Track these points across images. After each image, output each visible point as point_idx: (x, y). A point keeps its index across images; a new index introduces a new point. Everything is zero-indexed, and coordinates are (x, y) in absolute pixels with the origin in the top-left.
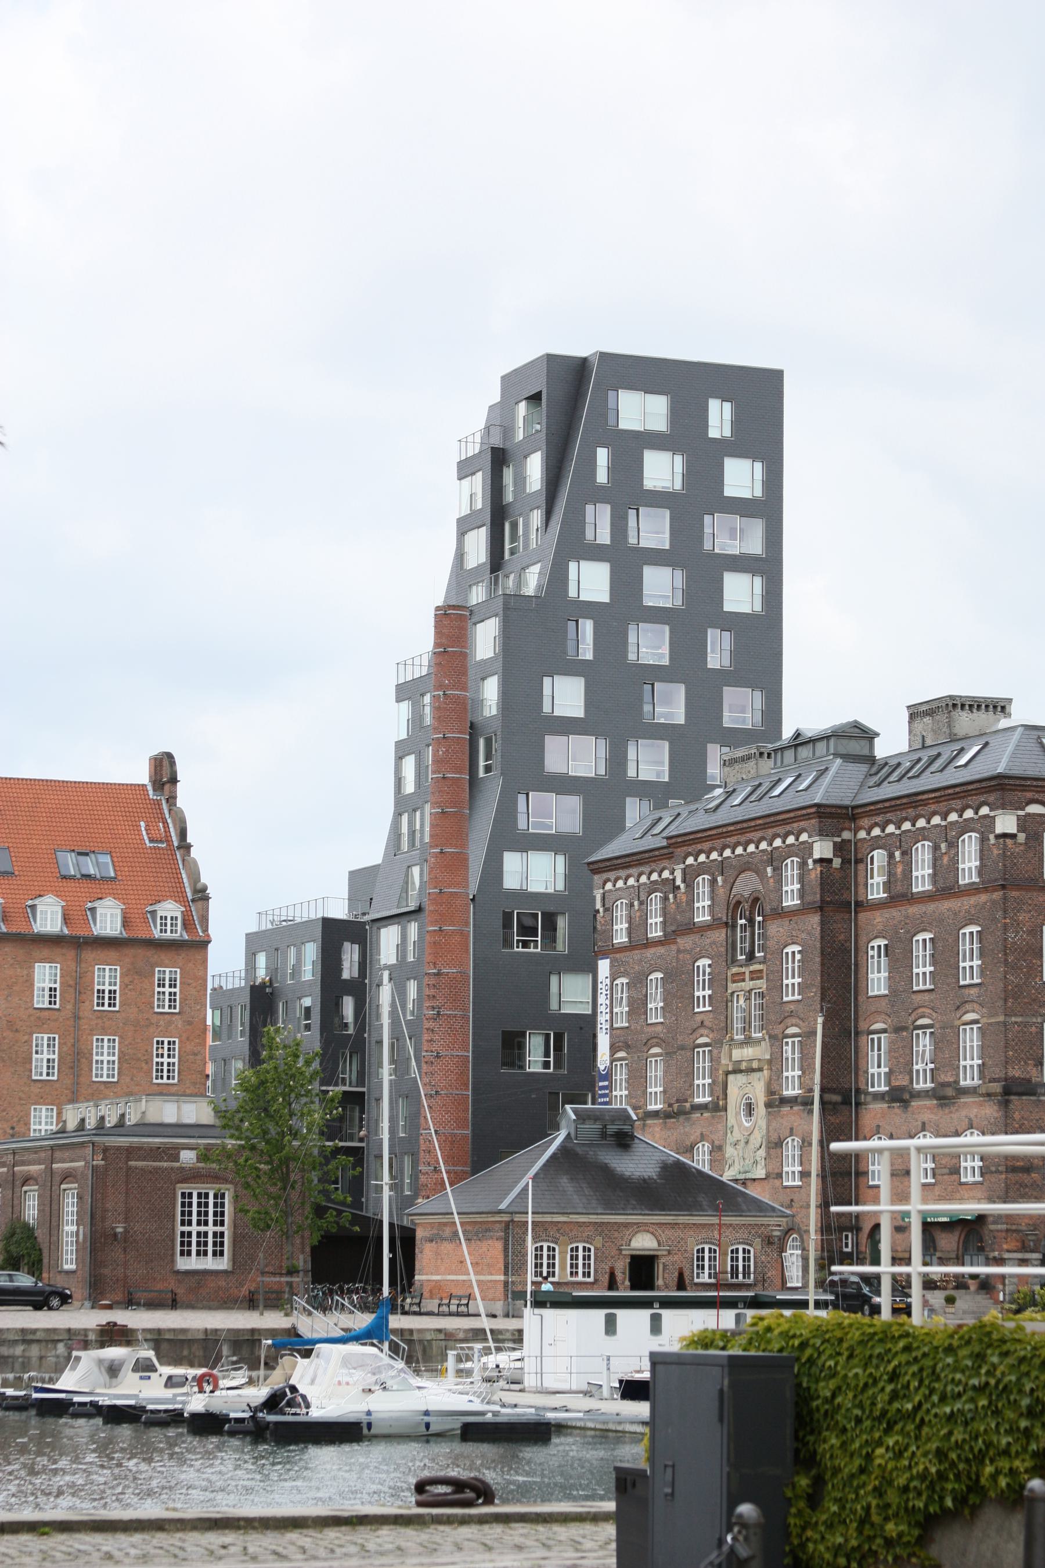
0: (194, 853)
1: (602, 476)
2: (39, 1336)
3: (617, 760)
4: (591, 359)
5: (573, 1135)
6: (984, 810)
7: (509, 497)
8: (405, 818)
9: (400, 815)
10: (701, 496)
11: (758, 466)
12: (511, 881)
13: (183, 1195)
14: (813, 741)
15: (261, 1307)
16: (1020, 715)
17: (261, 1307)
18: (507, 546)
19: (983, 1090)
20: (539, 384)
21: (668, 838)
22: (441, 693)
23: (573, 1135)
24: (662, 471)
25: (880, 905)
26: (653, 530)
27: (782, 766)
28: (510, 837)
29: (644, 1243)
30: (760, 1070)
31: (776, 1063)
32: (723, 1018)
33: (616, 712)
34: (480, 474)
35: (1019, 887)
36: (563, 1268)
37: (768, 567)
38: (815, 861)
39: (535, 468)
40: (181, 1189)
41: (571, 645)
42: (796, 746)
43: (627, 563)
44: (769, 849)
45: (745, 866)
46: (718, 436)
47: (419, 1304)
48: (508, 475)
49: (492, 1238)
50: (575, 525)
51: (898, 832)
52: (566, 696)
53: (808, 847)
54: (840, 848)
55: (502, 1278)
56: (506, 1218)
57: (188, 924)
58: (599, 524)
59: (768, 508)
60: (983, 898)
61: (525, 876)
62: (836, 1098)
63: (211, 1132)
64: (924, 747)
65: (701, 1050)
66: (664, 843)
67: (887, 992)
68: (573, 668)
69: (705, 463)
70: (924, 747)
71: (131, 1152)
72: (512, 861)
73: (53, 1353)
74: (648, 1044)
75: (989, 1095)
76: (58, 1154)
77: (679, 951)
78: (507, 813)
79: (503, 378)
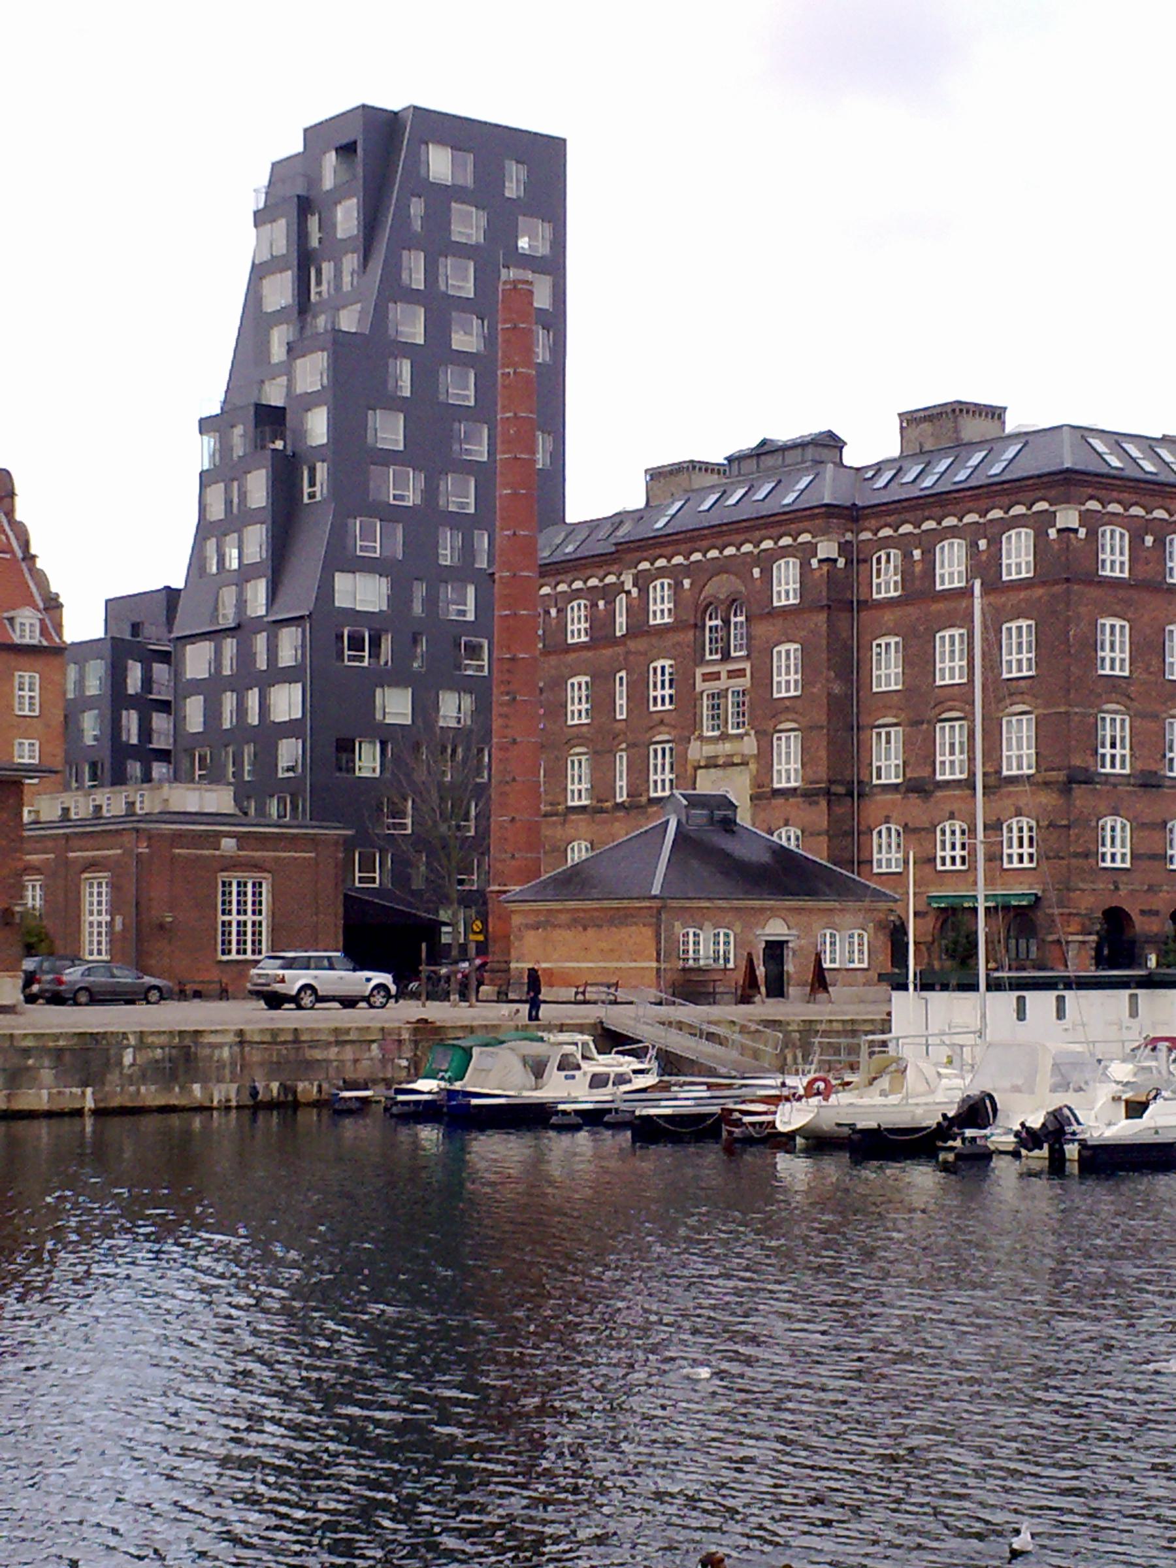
0: (39, 564)
1: (417, 225)
2: (353, 1036)
3: (431, 492)
5: (684, 820)
6: (805, 537)
7: (314, 243)
8: (211, 545)
9: (205, 539)
10: (495, 252)
13: (224, 883)
14: (785, 448)
15: (423, 998)
16: (1012, 424)
17: (423, 998)
19: (1039, 779)
20: (354, 132)
21: (616, 544)
22: (511, 371)
23: (684, 820)
25: (890, 603)
26: (461, 281)
27: (740, 474)
28: (342, 559)
29: (776, 929)
30: (745, 764)
31: (765, 757)
32: (691, 715)
33: (431, 449)
34: (282, 222)
35: (1080, 581)
36: (842, 953)
38: (820, 561)
39: (347, 218)
40: (223, 876)
42: (758, 455)
43: (440, 309)
44: (756, 551)
45: (722, 567)
47: (583, 993)
48: (313, 222)
49: (636, 924)
50: (393, 269)
51: (917, 531)
52: (389, 431)
53: (812, 549)
54: (844, 548)
55: (654, 965)
56: (656, 904)
57: (44, 632)
60: (1040, 591)
62: (840, 789)
63: (231, 820)
64: (921, 452)
65: (659, 747)
66: (613, 549)
67: (899, 687)
68: (393, 403)
70: (921, 452)
71: (177, 838)
73: (367, 1055)
74: (569, 743)
75: (1046, 784)
76: (75, 843)
77: (628, 653)
78: (339, 534)
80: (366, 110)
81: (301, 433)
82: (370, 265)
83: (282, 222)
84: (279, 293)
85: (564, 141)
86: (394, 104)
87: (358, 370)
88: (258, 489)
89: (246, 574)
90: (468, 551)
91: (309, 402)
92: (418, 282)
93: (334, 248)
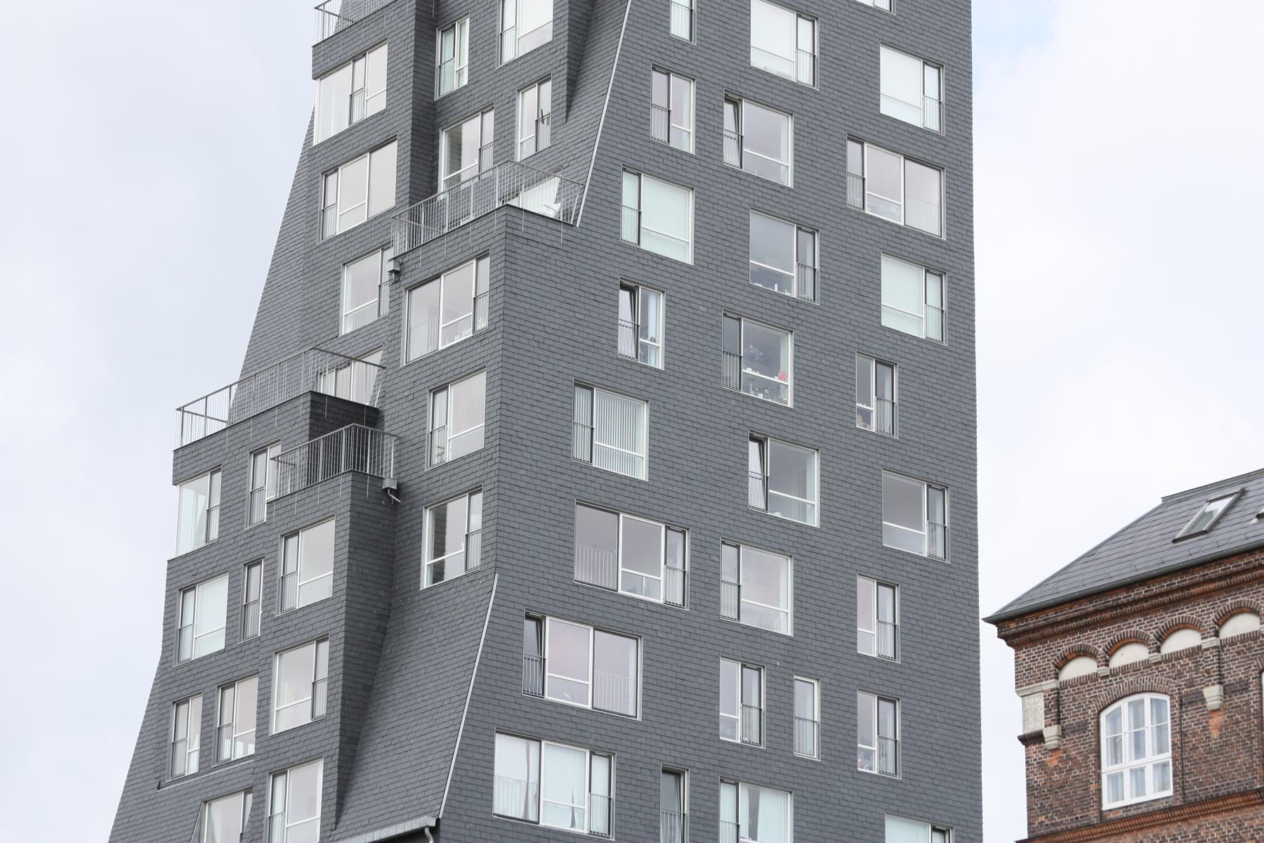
3: (703, 580)
11: (727, 610)
12: (507, 802)
26: (768, 145)
41: (530, 668)
46: (585, 832)
52: (619, 439)
58: (676, 110)
59: (945, 151)
61: (533, 792)
68: (630, 380)
72: (510, 757)
81: (416, 443)
83: (378, 59)
84: (368, 187)
87: (558, 289)
88: (313, 569)
89: (278, 755)
90: (779, 714)
91: (441, 373)
92: (685, 139)
93: (496, 86)
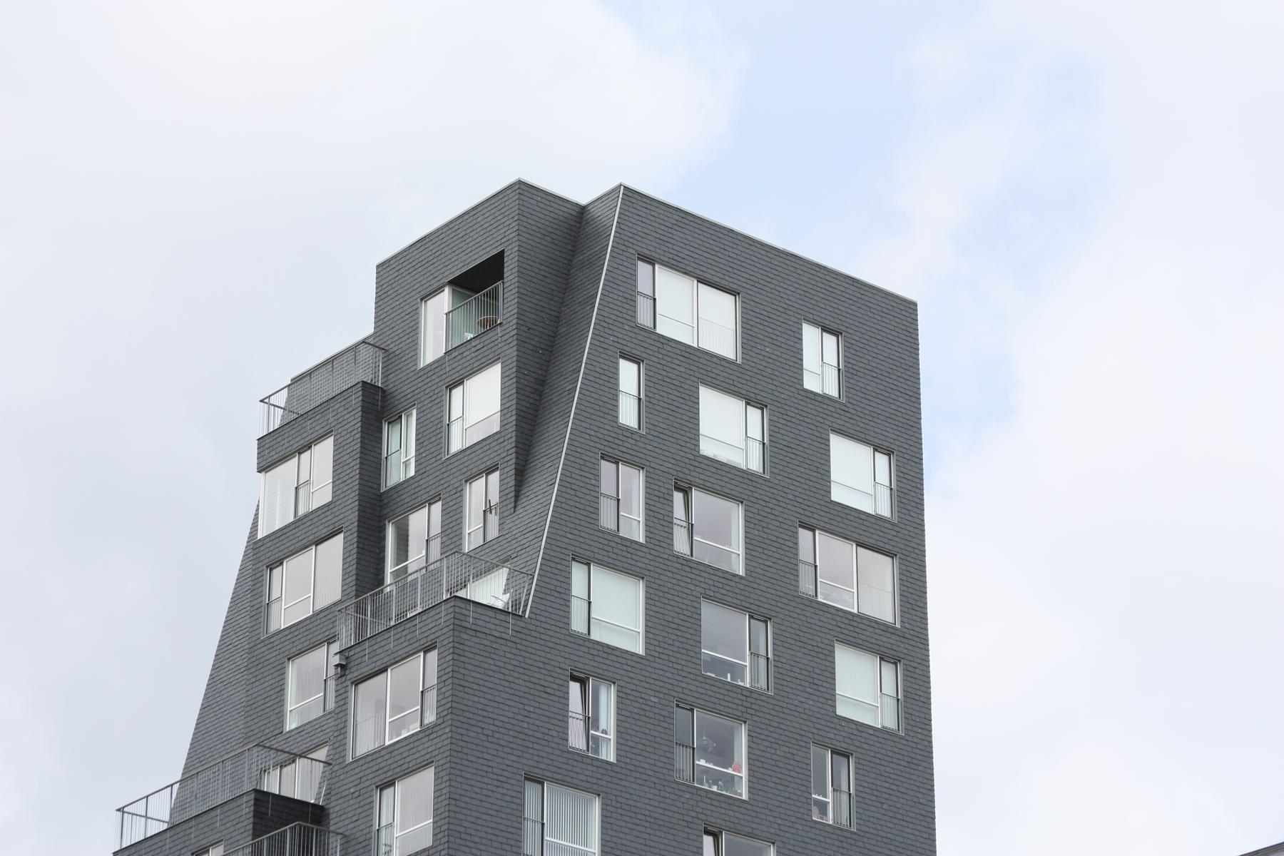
1: (628, 414)
4: (596, 212)
10: (788, 497)
18: (390, 568)
24: (729, 430)
26: (719, 534)
37: (902, 645)
43: (677, 589)
46: (818, 390)
50: (582, 498)
58: (626, 498)
59: (898, 537)
69: (800, 430)
79: (383, 268)
80: (522, 193)
82: (523, 500)
85: (915, 304)
86: (581, 188)
91: (389, 768)
92: (635, 529)
93: (443, 476)
